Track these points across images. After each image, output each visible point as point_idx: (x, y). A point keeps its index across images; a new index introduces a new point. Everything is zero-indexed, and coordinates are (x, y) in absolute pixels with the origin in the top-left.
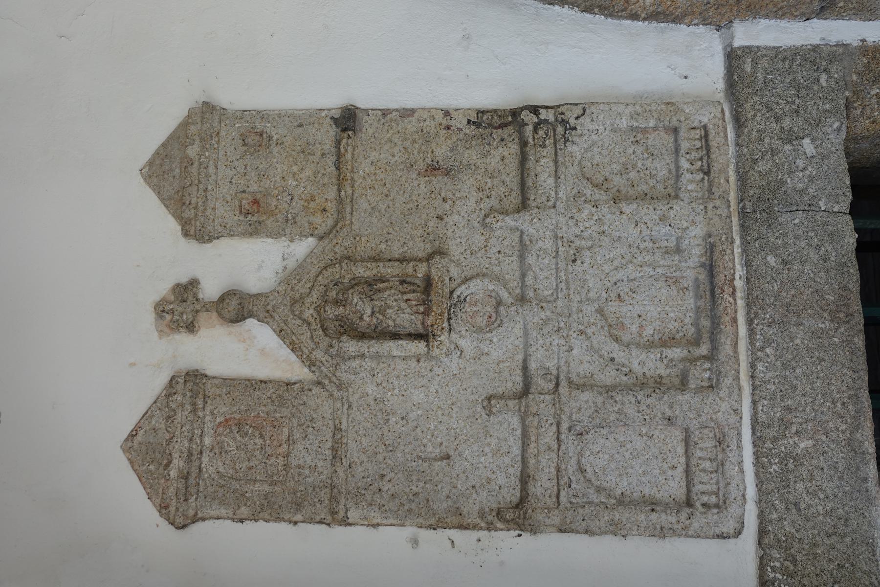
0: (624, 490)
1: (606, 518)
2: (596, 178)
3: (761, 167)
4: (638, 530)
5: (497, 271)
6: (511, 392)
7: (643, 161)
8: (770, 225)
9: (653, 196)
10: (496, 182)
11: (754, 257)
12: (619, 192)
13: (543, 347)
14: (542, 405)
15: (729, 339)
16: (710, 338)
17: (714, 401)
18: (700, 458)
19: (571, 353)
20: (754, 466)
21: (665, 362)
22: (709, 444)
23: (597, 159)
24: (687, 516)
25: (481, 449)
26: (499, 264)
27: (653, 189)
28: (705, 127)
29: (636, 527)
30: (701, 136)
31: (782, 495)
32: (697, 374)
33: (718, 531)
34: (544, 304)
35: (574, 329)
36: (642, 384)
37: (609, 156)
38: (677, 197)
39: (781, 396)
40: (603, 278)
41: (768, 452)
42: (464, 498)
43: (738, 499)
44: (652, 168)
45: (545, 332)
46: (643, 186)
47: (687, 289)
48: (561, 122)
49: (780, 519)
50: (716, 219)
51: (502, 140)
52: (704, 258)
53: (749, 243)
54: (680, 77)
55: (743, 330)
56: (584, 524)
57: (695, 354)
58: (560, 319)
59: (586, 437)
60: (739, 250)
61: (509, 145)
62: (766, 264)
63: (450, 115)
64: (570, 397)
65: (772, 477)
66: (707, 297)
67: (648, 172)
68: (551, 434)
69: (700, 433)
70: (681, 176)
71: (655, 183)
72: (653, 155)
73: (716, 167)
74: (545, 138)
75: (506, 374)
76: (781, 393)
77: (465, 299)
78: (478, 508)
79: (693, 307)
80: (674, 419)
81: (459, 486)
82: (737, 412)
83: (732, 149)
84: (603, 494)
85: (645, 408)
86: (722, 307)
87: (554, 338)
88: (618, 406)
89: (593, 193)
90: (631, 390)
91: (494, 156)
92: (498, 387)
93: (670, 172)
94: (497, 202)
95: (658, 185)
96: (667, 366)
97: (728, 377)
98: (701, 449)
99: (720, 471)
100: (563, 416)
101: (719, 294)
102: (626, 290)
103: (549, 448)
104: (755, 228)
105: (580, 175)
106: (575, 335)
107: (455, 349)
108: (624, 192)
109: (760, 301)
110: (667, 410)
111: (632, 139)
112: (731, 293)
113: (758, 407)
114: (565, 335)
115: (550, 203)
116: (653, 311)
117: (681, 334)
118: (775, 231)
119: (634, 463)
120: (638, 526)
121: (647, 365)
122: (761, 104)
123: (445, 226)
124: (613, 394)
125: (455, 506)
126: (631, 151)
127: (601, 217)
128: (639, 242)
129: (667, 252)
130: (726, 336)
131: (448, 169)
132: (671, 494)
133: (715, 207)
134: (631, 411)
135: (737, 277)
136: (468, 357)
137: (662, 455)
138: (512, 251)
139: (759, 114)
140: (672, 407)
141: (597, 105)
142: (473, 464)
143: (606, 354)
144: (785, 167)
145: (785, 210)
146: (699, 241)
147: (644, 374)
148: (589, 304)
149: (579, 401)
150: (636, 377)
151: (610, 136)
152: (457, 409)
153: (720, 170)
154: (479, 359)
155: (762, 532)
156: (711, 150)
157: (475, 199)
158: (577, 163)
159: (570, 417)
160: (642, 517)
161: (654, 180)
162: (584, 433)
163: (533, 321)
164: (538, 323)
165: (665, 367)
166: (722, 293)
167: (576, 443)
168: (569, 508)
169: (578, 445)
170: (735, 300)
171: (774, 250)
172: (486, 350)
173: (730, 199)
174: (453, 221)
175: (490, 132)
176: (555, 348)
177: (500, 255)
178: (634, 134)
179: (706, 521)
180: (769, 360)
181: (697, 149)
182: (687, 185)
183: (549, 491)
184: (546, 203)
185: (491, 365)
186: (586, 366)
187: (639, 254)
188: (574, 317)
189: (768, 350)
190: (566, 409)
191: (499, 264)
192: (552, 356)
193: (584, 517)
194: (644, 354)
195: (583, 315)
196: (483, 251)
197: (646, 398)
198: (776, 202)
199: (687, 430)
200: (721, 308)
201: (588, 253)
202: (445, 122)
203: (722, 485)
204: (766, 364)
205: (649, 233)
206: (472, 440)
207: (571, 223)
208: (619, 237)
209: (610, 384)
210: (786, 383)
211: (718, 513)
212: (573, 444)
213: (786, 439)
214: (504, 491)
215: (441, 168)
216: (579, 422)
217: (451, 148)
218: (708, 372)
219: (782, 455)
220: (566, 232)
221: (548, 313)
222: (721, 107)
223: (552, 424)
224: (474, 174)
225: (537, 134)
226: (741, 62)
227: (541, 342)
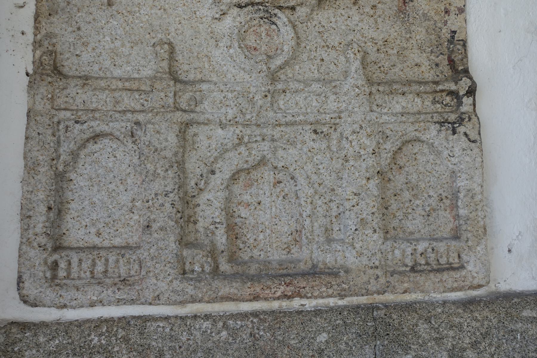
0: (75, 181)
1: (41, 158)
2: (401, 158)
3: (423, 327)
4: (28, 192)
5: (303, 57)
6: (178, 69)
7: (421, 205)
8: (360, 336)
9: (386, 216)
10: (394, 58)
11: (325, 319)
12: (388, 181)
13: (224, 97)
14: (162, 95)
15: (236, 291)
16: (237, 273)
17: (169, 275)
18: (107, 260)
19: (219, 127)
20: (98, 318)
21: (212, 227)
22: (123, 271)
23: (422, 159)
24: (43, 244)
25: (118, 37)
26: (309, 59)
27: (392, 216)
28: (462, 267)
29: (31, 189)
30: (451, 264)
31: (66, 348)
32: (198, 258)
33: (25, 277)
34: (269, 99)
35: (244, 130)
36: (187, 202)
37: (425, 172)
38: (386, 239)
39: (175, 346)
40: (299, 163)
41: (113, 333)
42: (67, 19)
43: (61, 299)
44: (415, 215)
45: (240, 100)
46: (395, 205)
47: (289, 252)
48: (461, 118)
49: (38, 345)
50: (365, 279)
51: (437, 65)
52: (322, 267)
53: (340, 314)
54: (509, 245)
55: (246, 307)
56: (34, 134)
57: (220, 257)
58: (254, 115)
59: (129, 141)
60: (332, 304)
61: (432, 72)
62: (319, 332)
63: (460, 13)
64: (171, 123)
65: (85, 337)
66: (282, 271)
67: (410, 211)
68: (133, 105)
69: (134, 260)
70: (408, 242)
71: (399, 217)
72: (428, 216)
73: (420, 279)
74: (443, 103)
75: (197, 64)
76: (178, 347)
77: (274, 23)
78: (57, 32)
79: (270, 258)
80: (148, 232)
81: (80, 14)
82: (156, 300)
83: (438, 296)
84: (69, 158)
85: (161, 201)
86: (270, 284)
87: (235, 109)
88: (162, 173)
89: (387, 151)
90: (179, 187)
91: (420, 56)
92: (183, 56)
93: (412, 233)
94: (373, 59)
95: (398, 221)
96: (206, 229)
97: (194, 289)
98: (117, 261)
99: (92, 281)
100: (150, 115)
101: (284, 281)
102: (286, 189)
103: (117, 102)
104: (357, 320)
105: (406, 138)
106: (238, 132)
107: (222, 10)
108: (388, 185)
109: (278, 325)
110: (158, 225)
111: (444, 194)
112: (286, 293)
113: (162, 321)
114: (237, 120)
115: (375, 108)
116: (265, 217)
117: (241, 246)
118: (354, 341)
119: (103, 193)
120: (32, 192)
121: (208, 208)
122: (489, 327)
123: (347, 7)
124: (175, 168)
125: (59, 10)
126: (431, 193)
127: (363, 157)
128: (337, 202)
129: (327, 230)
130: (239, 288)
131: (405, 11)
132: (71, 231)
133: (378, 277)
134: (157, 186)
135: (304, 301)
136: (213, 26)
137: (112, 222)
138: (324, 72)
139: (478, 324)
140: (161, 230)
141: (480, 154)
142: (102, 29)
143: (218, 166)
144: (423, 353)
145: (377, 352)
146: (340, 261)
147: (198, 205)
148: (271, 148)
149: (167, 132)
150: (194, 196)
151: (446, 172)
152: (159, 14)
153: (417, 283)
154: (212, 38)
155: (24, 326)
156: (438, 274)
157: (375, 38)
158: (417, 135)
159: (149, 122)
160: (41, 196)
161: (402, 217)
162: (134, 139)
163: (251, 88)
164: (250, 93)
165: (206, 227)
166: (285, 283)
167: (123, 130)
168: (53, 120)
169: (121, 133)
170: (278, 298)
171: (333, 340)
172: (221, 44)
173: (386, 294)
174: (353, 15)
175: (444, 53)
176: (223, 110)
177: (319, 61)
178: (449, 196)
179: (37, 264)
180: (213, 334)
181: (438, 260)
182: (399, 248)
183: (71, 101)
184: (375, 103)
185: (205, 49)
186: (206, 143)
187: (325, 201)
188: (257, 131)
189: (224, 333)
190: (158, 118)
191: (309, 59)
192: (215, 107)
193: (42, 134)
194: (219, 205)
195: (259, 142)
196: (323, 44)
197: (171, 203)
198: (386, 342)
199: (139, 247)
200: (269, 283)
201: (324, 146)
202: (452, 8)
203: (78, 282)
204: (209, 331)
205: (348, 208)
206: (127, 28)
207: (356, 127)
208: (342, 178)
209: (187, 167)
210: (189, 352)
211: (46, 278)
212: (122, 127)
213: (127, 352)
214: (75, 60)
215: (406, 4)
216: (145, 132)
217: (426, 14)
218: (201, 269)
219: (110, 348)
220: (345, 122)
221: (260, 102)
222: (484, 284)
223: (143, 105)
224: (401, 37)
225: (447, 95)
226: (533, 306)
227: (230, 95)
